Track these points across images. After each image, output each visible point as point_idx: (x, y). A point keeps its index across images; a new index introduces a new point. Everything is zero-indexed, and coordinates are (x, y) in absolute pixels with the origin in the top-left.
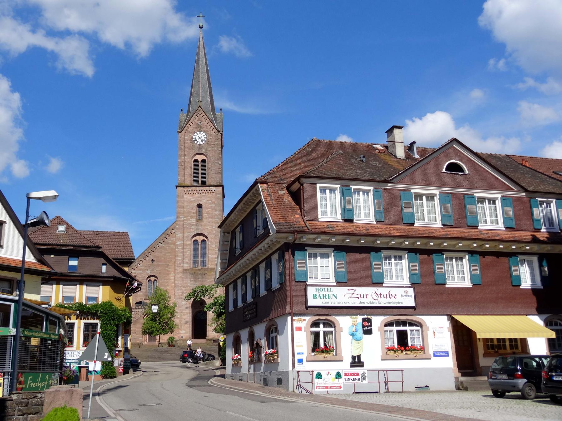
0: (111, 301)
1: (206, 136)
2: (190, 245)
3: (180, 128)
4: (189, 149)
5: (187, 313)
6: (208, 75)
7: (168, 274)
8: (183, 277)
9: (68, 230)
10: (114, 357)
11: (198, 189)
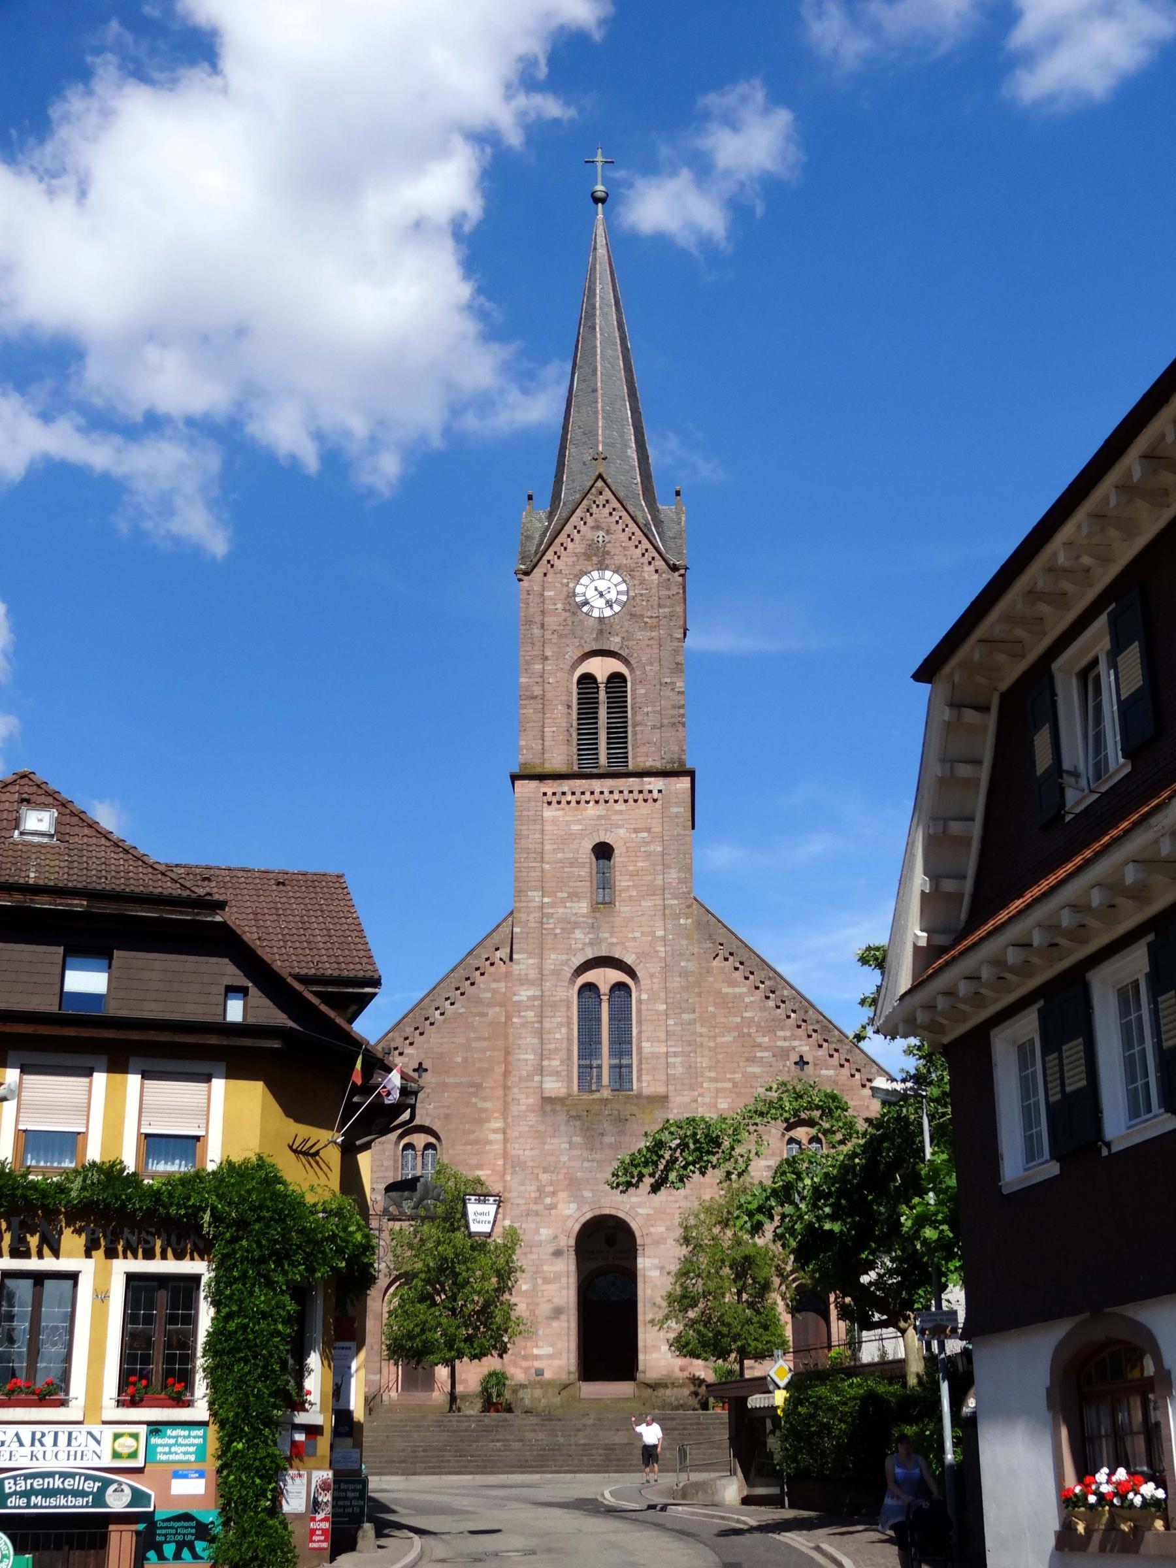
0: (268, 1160)
1: (623, 587)
2: (568, 1002)
3: (523, 559)
4: (561, 636)
5: (557, 1277)
6: (628, 369)
7: (480, 1122)
8: (541, 1128)
9: (67, 829)
10: (282, 1463)
11: (597, 785)
